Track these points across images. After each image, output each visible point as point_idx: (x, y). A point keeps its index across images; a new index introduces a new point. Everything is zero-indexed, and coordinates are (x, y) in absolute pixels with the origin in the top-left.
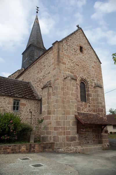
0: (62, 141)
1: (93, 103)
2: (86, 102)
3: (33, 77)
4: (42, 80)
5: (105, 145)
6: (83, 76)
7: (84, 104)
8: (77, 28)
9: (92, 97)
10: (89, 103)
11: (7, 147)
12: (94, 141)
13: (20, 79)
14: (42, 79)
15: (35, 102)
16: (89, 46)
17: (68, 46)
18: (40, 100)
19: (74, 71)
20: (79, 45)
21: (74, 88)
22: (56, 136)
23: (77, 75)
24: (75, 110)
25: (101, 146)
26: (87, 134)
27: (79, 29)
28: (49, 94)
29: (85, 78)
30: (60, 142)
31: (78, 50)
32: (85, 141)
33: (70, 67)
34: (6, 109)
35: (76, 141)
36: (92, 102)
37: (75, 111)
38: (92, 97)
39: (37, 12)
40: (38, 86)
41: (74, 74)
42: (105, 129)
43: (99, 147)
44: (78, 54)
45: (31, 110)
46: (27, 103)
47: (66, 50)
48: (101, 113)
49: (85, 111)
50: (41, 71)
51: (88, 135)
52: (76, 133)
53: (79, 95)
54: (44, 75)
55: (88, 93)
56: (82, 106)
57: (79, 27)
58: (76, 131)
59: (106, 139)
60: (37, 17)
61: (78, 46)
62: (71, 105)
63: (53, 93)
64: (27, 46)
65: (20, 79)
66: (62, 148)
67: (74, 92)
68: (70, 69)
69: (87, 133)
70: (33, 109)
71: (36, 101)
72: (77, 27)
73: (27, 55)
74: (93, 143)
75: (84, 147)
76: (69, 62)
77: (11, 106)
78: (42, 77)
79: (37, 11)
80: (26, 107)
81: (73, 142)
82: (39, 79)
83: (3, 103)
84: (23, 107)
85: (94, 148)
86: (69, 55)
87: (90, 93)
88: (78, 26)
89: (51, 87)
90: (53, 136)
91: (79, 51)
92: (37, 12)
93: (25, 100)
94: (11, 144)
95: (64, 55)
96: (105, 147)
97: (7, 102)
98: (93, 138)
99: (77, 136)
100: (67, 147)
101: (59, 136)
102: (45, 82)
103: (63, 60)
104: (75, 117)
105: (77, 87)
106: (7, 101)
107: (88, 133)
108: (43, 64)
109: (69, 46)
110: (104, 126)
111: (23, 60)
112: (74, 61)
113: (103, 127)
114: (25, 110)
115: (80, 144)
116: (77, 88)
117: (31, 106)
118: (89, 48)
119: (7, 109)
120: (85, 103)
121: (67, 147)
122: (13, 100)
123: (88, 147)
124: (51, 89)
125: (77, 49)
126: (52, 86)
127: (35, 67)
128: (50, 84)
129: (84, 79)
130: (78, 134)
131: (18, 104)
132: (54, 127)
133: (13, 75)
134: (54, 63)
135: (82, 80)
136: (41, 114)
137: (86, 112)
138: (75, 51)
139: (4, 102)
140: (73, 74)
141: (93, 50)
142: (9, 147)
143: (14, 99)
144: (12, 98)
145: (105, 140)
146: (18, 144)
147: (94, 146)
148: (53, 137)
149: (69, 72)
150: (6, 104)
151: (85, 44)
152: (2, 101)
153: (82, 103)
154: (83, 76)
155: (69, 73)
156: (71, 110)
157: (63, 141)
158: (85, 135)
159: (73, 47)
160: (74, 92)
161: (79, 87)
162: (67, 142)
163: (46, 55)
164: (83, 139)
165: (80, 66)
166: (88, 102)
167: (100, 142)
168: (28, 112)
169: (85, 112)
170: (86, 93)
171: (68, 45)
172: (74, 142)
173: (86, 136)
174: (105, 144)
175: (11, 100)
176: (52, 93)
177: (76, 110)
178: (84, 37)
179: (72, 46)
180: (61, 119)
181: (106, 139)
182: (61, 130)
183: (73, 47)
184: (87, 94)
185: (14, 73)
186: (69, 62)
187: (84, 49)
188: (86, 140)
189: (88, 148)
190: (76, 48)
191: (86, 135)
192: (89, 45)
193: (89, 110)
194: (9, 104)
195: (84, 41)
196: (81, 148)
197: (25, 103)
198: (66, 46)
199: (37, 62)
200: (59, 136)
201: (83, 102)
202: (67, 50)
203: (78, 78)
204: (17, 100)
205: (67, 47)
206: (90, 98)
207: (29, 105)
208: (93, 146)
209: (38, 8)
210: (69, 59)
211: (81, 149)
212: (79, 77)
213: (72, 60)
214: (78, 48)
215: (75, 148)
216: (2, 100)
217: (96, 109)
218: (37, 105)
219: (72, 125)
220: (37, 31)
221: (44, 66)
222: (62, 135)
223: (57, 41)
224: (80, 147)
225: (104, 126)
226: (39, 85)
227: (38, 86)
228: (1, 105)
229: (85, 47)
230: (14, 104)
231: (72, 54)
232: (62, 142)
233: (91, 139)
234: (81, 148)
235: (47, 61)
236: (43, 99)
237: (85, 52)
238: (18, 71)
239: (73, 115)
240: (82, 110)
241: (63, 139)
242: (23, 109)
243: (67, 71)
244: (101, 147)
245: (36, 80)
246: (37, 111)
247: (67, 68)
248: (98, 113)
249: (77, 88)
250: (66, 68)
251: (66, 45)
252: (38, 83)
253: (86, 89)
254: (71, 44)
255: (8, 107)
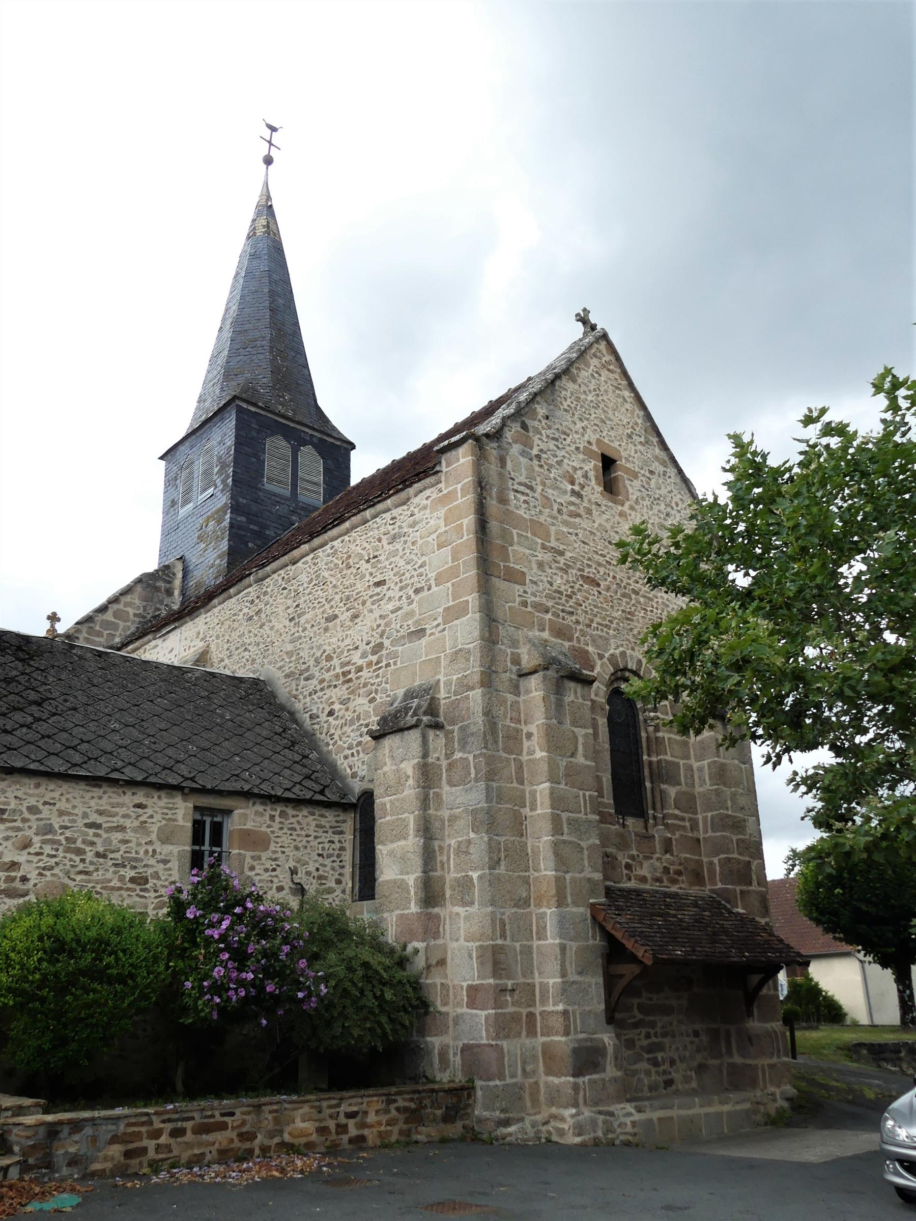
0: (519, 1072)
1: (687, 824)
2: (646, 822)
3: (289, 647)
4: (365, 674)
5: (773, 1094)
6: (623, 654)
7: (637, 835)
8: (578, 330)
9: (679, 784)
10: (667, 826)
11: (213, 1116)
12: (701, 1068)
13: (171, 649)
14: (360, 669)
15: (323, 821)
16: (657, 450)
17: (536, 462)
18: (363, 808)
19: (570, 620)
20: (594, 448)
21: (580, 732)
22: (479, 1046)
23: (590, 649)
24: (590, 876)
25: (747, 1106)
26: (658, 1029)
27: (595, 344)
28: (427, 775)
29: (639, 662)
30: (509, 1081)
31: (593, 482)
32: (648, 1073)
33: (548, 597)
34: (150, 871)
35: (604, 1070)
36: (683, 819)
37: (589, 880)
38: (679, 784)
39: (268, 161)
40: (331, 713)
41: (575, 643)
42: (764, 991)
43: (739, 1107)
44: (589, 512)
45: (301, 877)
46: (276, 826)
47: (522, 488)
48: (738, 888)
49: (643, 879)
50: (356, 616)
51: (664, 1035)
52: (603, 1018)
53: (607, 778)
54: (380, 646)
55: (654, 759)
56: (623, 844)
57: (593, 327)
58: (603, 1007)
59: (775, 1060)
60: (269, 198)
61: (588, 453)
62: (564, 842)
63: (451, 766)
64: (201, 400)
65: (171, 649)
66: (521, 1120)
67: (580, 759)
68: (547, 612)
69: (661, 1021)
70: (311, 868)
71: (324, 811)
72: (580, 324)
73: (207, 473)
74: (694, 1084)
75: (654, 1109)
76: (541, 565)
77: (180, 855)
78: (364, 655)
79: (264, 149)
80: (269, 854)
81: (587, 1078)
82: (343, 665)
83: (129, 835)
84: (249, 854)
85: (707, 1115)
86: (542, 519)
87: (668, 758)
88: (583, 319)
89: (438, 726)
90: (460, 1044)
91: (594, 491)
92: (268, 161)
93: (260, 808)
94: (136, 1107)
95: (519, 522)
96: (772, 1109)
97: (155, 828)
98: (698, 1050)
99: (607, 1038)
100: (554, 1110)
101: (505, 1044)
102: (393, 690)
103: (506, 559)
104: (594, 918)
105: (595, 726)
106: (157, 817)
107: (666, 1019)
108: (364, 566)
109: (538, 457)
110: (761, 976)
111: (171, 505)
112: (568, 555)
113: (755, 979)
114: (266, 876)
115: (628, 1092)
116: (595, 735)
117: (297, 848)
118: (657, 458)
119: (156, 876)
120: (640, 823)
121: (554, 1110)
122: (191, 811)
123: (671, 1108)
124: (437, 741)
125: (586, 476)
126: (441, 719)
127: (304, 578)
128: (432, 710)
129: (631, 671)
130: (610, 1028)
131: (217, 840)
132: (470, 988)
133: (109, 616)
134: (453, 572)
135: (617, 679)
136: (372, 897)
137: (648, 887)
138: (577, 488)
139: (135, 830)
140: (567, 644)
141: (680, 472)
142: (222, 1115)
143: (196, 808)
144: (185, 801)
145: (772, 1067)
146: (274, 1103)
147: (710, 1105)
148: (462, 1051)
149: (543, 630)
150: (150, 843)
151: (630, 436)
152: (128, 823)
153: (624, 826)
154: (623, 654)
155: (546, 635)
156: (568, 876)
157: (524, 1070)
158: (648, 1036)
159: (559, 463)
160: (580, 759)
161: (602, 722)
162: (550, 1078)
163: (388, 510)
164: (639, 1059)
165: (608, 589)
166: (655, 818)
167: (740, 1079)
168: (280, 889)
169: (643, 886)
170: (645, 757)
171: (535, 451)
172: (595, 1076)
173: (654, 1039)
174: (772, 1089)
175: (180, 814)
176: (444, 763)
177: (598, 876)
178: (627, 394)
179: (553, 461)
180: (508, 933)
181: (775, 1060)
182: (513, 1004)
183: (559, 463)
184: (650, 763)
185: (114, 600)
186: (541, 565)
187: (627, 471)
188: (656, 1063)
189: (674, 1113)
190: (579, 473)
191: (656, 1035)
192: (655, 440)
193: (666, 870)
194: (165, 838)
195: (626, 415)
196: (637, 1117)
197: (264, 829)
198: (524, 461)
199: (322, 546)
200: (505, 1044)
201: (630, 821)
202: (531, 488)
203: (599, 663)
204: (212, 811)
205: (530, 469)
206: (672, 791)
207: (286, 840)
208: (701, 1106)
209: (273, 129)
210: (544, 547)
211: (634, 1123)
212: (601, 657)
213: (562, 553)
214: (593, 466)
215: (601, 1117)
216: (125, 816)
217: (711, 863)
218: (336, 838)
219: (580, 973)
220: (272, 294)
221: (378, 584)
222: (519, 1035)
223: (780, 764)
224: (630, 1108)
225: (761, 976)
226: (336, 707)
227: (331, 713)
228: (123, 848)
229: (632, 455)
230: (197, 838)
231: (555, 512)
232: (519, 1079)
233: (682, 1059)
234: (637, 1117)
235: (395, 553)
236: (382, 801)
237: (633, 488)
238: (139, 581)
239: (581, 910)
240: (625, 872)
241: (524, 1063)
242: (252, 868)
243: (531, 627)
244: (747, 1112)
245: (315, 671)
246: (339, 882)
247: (536, 606)
248: (720, 885)
249: (595, 735)
250: (525, 604)
251: (523, 453)
252: (335, 694)
253: (643, 734)
254: (551, 445)
255: (165, 862)
